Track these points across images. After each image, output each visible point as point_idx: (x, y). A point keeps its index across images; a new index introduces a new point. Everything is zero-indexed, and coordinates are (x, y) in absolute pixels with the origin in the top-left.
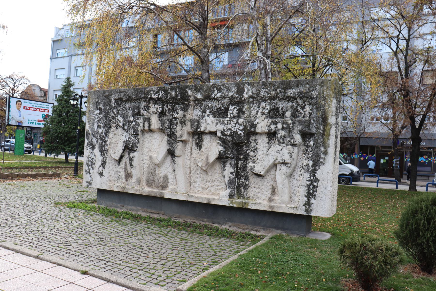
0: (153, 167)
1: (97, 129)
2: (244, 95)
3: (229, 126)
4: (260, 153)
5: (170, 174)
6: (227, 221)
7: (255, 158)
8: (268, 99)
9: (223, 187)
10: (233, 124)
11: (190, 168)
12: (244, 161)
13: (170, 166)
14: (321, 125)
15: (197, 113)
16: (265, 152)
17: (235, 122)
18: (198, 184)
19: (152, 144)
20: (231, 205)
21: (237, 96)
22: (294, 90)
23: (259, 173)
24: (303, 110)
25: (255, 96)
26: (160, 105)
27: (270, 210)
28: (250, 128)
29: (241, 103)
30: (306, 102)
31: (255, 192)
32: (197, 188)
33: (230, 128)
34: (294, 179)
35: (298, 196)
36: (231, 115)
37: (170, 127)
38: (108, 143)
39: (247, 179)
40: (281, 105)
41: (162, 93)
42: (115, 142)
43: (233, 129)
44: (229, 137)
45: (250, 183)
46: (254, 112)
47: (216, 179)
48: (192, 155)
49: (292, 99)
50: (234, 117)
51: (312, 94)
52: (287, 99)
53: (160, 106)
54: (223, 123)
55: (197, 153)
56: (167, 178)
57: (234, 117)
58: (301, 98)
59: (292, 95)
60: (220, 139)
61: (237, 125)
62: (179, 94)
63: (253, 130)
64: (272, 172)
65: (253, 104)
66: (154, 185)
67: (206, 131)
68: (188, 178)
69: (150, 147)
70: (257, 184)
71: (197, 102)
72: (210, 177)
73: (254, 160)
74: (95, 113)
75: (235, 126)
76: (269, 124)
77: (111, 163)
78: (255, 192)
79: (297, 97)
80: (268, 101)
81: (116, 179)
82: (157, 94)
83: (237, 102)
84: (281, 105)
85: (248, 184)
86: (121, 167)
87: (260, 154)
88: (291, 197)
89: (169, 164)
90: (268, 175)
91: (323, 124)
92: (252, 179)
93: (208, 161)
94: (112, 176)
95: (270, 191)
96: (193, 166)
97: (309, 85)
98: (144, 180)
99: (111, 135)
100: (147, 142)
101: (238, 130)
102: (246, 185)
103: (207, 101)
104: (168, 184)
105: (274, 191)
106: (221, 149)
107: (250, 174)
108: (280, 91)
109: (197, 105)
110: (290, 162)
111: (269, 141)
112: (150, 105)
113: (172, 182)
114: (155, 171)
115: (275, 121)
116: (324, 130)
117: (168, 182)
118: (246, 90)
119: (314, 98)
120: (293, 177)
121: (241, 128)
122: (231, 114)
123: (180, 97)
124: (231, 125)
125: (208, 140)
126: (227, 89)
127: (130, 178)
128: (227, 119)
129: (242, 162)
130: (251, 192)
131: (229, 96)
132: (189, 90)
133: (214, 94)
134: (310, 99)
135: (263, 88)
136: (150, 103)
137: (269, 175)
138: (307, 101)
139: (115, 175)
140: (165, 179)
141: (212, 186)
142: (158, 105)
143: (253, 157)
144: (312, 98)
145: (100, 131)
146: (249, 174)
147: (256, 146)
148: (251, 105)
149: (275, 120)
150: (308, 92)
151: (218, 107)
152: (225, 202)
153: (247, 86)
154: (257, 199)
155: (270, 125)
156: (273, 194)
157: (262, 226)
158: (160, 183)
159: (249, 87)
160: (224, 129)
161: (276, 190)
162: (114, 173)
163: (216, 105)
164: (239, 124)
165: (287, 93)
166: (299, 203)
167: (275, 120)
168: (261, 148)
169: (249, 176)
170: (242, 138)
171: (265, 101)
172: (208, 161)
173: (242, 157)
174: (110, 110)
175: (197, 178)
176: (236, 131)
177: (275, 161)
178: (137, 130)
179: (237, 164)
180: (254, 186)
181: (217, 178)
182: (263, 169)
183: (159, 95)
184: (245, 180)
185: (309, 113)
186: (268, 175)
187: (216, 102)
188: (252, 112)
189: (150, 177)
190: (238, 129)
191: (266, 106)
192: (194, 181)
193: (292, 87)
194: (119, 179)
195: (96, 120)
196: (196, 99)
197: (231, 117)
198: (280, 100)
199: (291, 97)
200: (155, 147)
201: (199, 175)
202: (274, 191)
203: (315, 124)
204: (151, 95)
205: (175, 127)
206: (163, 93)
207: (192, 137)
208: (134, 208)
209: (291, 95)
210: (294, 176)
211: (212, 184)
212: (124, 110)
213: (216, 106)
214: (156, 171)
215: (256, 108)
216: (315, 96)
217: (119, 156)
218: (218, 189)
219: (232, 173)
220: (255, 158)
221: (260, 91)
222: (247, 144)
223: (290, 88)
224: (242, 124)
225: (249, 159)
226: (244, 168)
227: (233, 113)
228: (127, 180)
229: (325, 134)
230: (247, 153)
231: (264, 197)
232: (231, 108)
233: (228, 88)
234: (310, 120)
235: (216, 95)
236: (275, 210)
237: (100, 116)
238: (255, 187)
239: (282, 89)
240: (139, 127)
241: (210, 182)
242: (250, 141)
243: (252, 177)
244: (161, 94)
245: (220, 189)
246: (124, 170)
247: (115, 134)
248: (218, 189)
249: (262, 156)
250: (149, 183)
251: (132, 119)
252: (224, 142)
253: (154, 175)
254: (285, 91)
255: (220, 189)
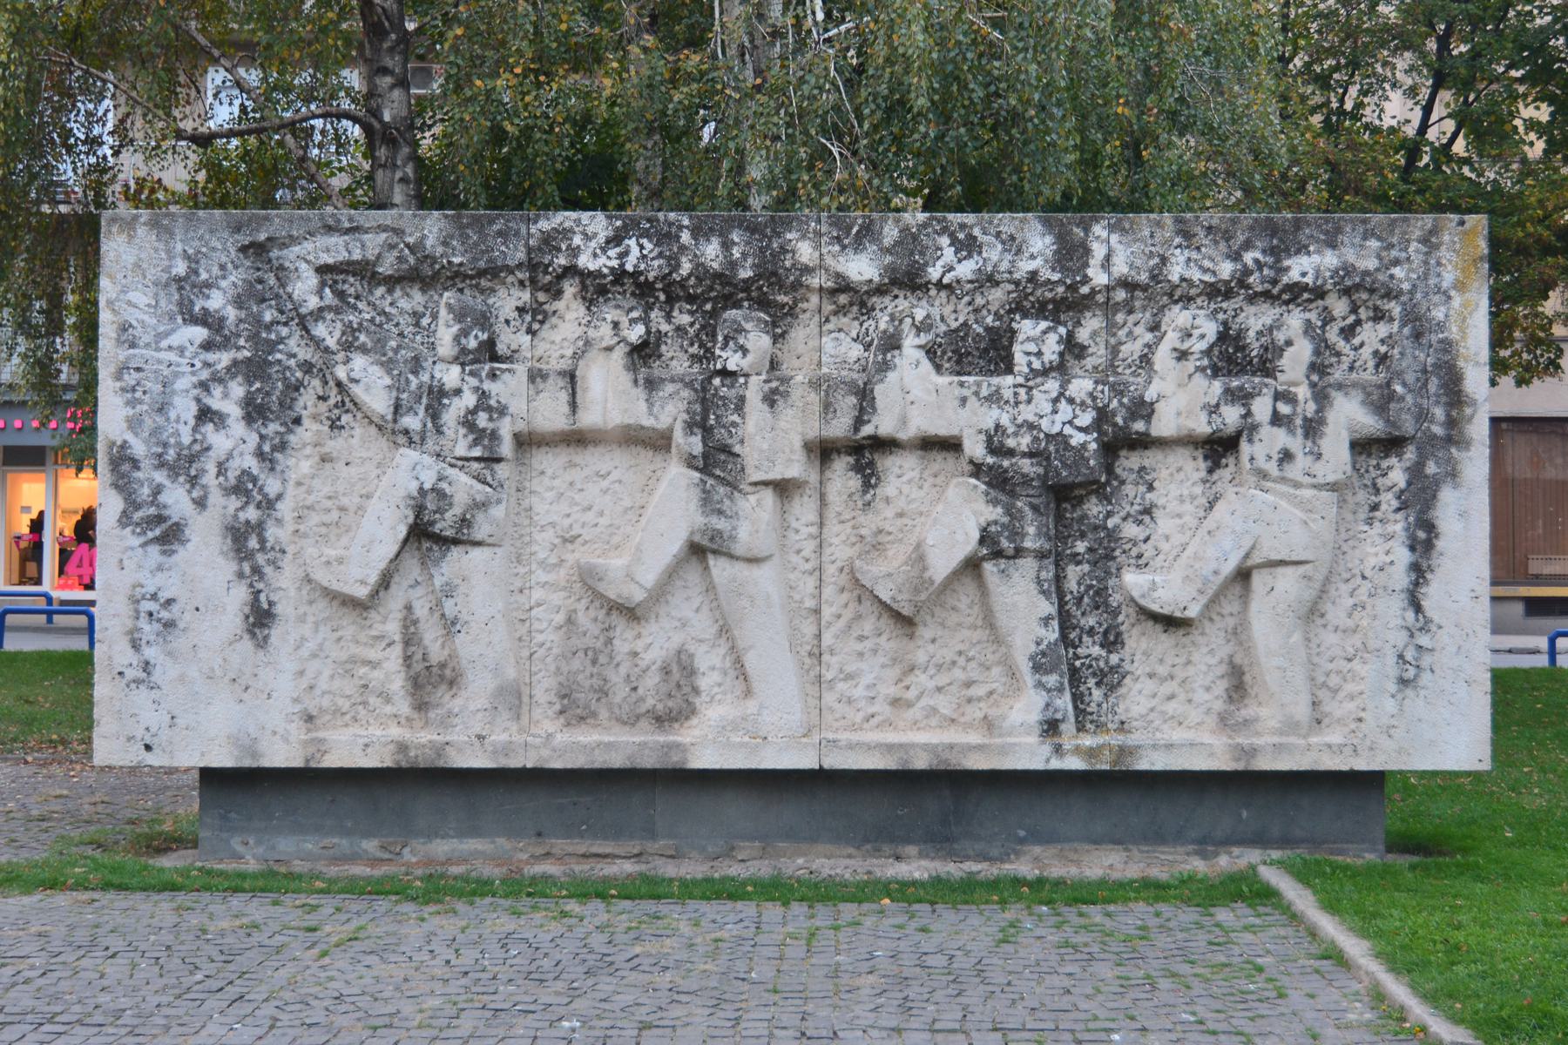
0: (596, 620)
1: (195, 430)
2: (1090, 272)
3: (1027, 413)
4: (1164, 524)
5: (704, 648)
6: (1022, 841)
7: (1148, 551)
8: (1199, 295)
9: (994, 686)
10: (1042, 403)
11: (817, 611)
12: (1094, 564)
13: (697, 610)
14: (1437, 403)
15: (843, 349)
16: (1190, 520)
17: (1054, 394)
18: (868, 687)
19: (586, 504)
20: (1056, 764)
21: (1056, 277)
22: (1316, 258)
23: (1178, 614)
24: (1347, 340)
25: (1144, 277)
26: (631, 310)
27: (1240, 766)
28: (1125, 420)
29: (1069, 308)
30: (1362, 310)
31: (1154, 696)
32: (862, 704)
33: (1031, 418)
34: (1325, 626)
35: (1352, 697)
36: (1029, 364)
37: (705, 418)
38: (285, 508)
39: (1112, 641)
40: (1252, 321)
41: (642, 247)
42: (329, 504)
43: (1045, 424)
44: (1027, 461)
45: (1128, 658)
46: (1132, 350)
47: (960, 653)
48: (827, 551)
49: (1306, 296)
50: (1045, 372)
51: (1392, 277)
52: (1285, 297)
53: (635, 314)
54: (995, 398)
55: (853, 539)
56: (690, 671)
57: (1045, 372)
58: (1347, 292)
59: (1309, 280)
60: (977, 469)
61: (1063, 405)
62: (744, 255)
63: (1139, 426)
64: (1230, 606)
65: (1130, 312)
66: (604, 714)
67: (903, 436)
68: (808, 661)
69: (567, 522)
70: (1161, 661)
71: (843, 299)
72: (931, 648)
73: (1140, 556)
74: (175, 340)
75: (1055, 412)
76: (1213, 402)
77: (311, 619)
78: (1154, 696)
79: (1329, 287)
80: (1199, 301)
81: (345, 705)
82: (612, 253)
83: (1053, 300)
84: (1255, 319)
85: (1119, 666)
86: (377, 638)
87: (1167, 532)
88: (1314, 703)
89: (696, 602)
90: (1211, 620)
91: (1444, 399)
92: (1138, 641)
93: (927, 575)
94: (318, 692)
95: (1221, 687)
96: (835, 603)
97: (1379, 239)
98: (544, 689)
99: (299, 464)
100: (550, 495)
101: (1068, 430)
102: (1111, 668)
103: (896, 297)
104: (697, 701)
105: (1238, 683)
106: (992, 517)
107: (1126, 618)
108: (1257, 261)
109: (841, 311)
110: (1310, 558)
111: (1210, 471)
112: (559, 305)
113: (716, 689)
114: (609, 641)
115: (1241, 388)
116: (1451, 423)
117: (696, 691)
118: (1099, 250)
119: (1401, 293)
120: (1319, 622)
121: (1086, 419)
122: (1033, 359)
123: (750, 273)
124: (1031, 407)
125: (909, 475)
126: (1003, 243)
127: (444, 687)
128: (1009, 380)
129: (1086, 568)
130: (1136, 699)
131: (1017, 276)
132: (803, 237)
133: (940, 263)
134: (1382, 297)
135: (1179, 246)
136: (558, 294)
137: (1215, 617)
138: (1370, 304)
139: (337, 683)
140: (676, 674)
141: (939, 689)
142: (618, 307)
143: (1135, 545)
144: (1389, 295)
145: (220, 442)
146: (1121, 618)
147: (1148, 496)
148: (1120, 317)
149: (1235, 383)
150: (1377, 270)
151: (954, 325)
152: (1031, 755)
153: (1104, 234)
154: (1165, 727)
155: (1217, 406)
156: (1235, 696)
157: (1193, 842)
158: (642, 699)
159: (1114, 238)
160: (998, 426)
161: (1247, 678)
162: (327, 673)
163: (945, 313)
164: (1071, 401)
165: (1288, 269)
166: (1362, 725)
167: (1235, 383)
168: (1173, 506)
169: (1123, 628)
170: (1092, 462)
171: (1187, 300)
172: (927, 575)
173: (1081, 547)
174: (286, 324)
175: (861, 654)
176: (1060, 434)
177: (1247, 556)
178: (494, 436)
179: (1059, 579)
180: (1148, 670)
181: (961, 647)
182: (1195, 594)
183: (624, 255)
184: (1102, 646)
185: (1376, 353)
186: (1211, 620)
187: (945, 300)
188: (1123, 348)
189: (578, 672)
190: (1070, 422)
191: (1197, 322)
192: (841, 671)
193: (1306, 247)
194: (365, 703)
195: (183, 383)
196: (843, 286)
197: (1032, 370)
198: (1252, 299)
199: (1305, 288)
200: (603, 521)
201: (868, 644)
202: (1238, 683)
203: (1409, 399)
204: (575, 252)
205: (735, 418)
206: (648, 246)
207: (818, 463)
208: (480, 847)
209: (1305, 280)
210: (1322, 616)
211: (943, 680)
212: (380, 326)
213: (942, 319)
214: (616, 642)
215: (1138, 330)
216: (1406, 286)
217: (373, 578)
218: (969, 701)
219: (1046, 621)
220: (1144, 547)
221: (1164, 260)
222: (1100, 488)
223: (1298, 252)
224: (1089, 402)
225: (1117, 553)
226: (1100, 598)
227: (1039, 354)
228: (421, 706)
229: (1454, 436)
230: (1105, 528)
231: (1195, 715)
232: (1027, 328)
233: (1012, 238)
234: (1388, 384)
235: (951, 269)
236: (1264, 764)
237: (211, 357)
238: (1151, 676)
239: (1264, 252)
240: (507, 419)
241: (932, 671)
242: (1117, 477)
243: (1135, 631)
244: (635, 252)
245: (979, 699)
246: (397, 650)
247: (325, 459)
248: (969, 701)
249: (1177, 539)
250: (573, 709)
251: (451, 376)
252: (999, 482)
253: (602, 659)
254: (1278, 260)
255: (979, 699)
